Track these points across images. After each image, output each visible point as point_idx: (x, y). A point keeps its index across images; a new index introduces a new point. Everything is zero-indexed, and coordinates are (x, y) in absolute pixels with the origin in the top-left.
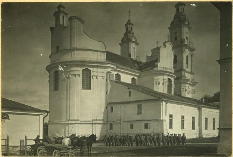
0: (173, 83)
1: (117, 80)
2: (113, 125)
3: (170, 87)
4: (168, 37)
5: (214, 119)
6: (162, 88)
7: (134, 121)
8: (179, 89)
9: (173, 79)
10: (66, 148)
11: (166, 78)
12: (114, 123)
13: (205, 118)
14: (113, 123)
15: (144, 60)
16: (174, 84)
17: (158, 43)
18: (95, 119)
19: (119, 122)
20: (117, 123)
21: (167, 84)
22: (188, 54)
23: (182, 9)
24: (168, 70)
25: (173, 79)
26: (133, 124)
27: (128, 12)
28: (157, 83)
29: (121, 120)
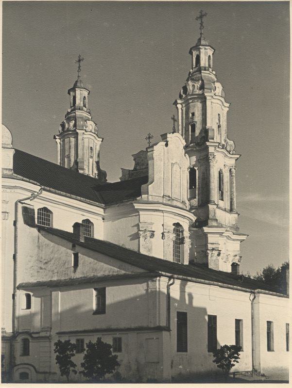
0: (187, 234)
1: (44, 223)
2: (30, 344)
3: (179, 242)
4: (172, 121)
5: (238, 322)
6: (159, 248)
7: (85, 332)
8: (202, 251)
9: (186, 225)
10: (122, 370)
11: (170, 221)
12: (32, 337)
13: (268, 322)
14: (29, 338)
15: (114, 178)
16: (190, 238)
17: (149, 138)
18: (48, 328)
19: (48, 334)
20: (42, 337)
21: (173, 236)
22: (222, 167)
23: (207, 58)
24: (175, 203)
25: (186, 225)
26: (120, 339)
27: (148, 136)
28: (148, 234)
29: (51, 328)
